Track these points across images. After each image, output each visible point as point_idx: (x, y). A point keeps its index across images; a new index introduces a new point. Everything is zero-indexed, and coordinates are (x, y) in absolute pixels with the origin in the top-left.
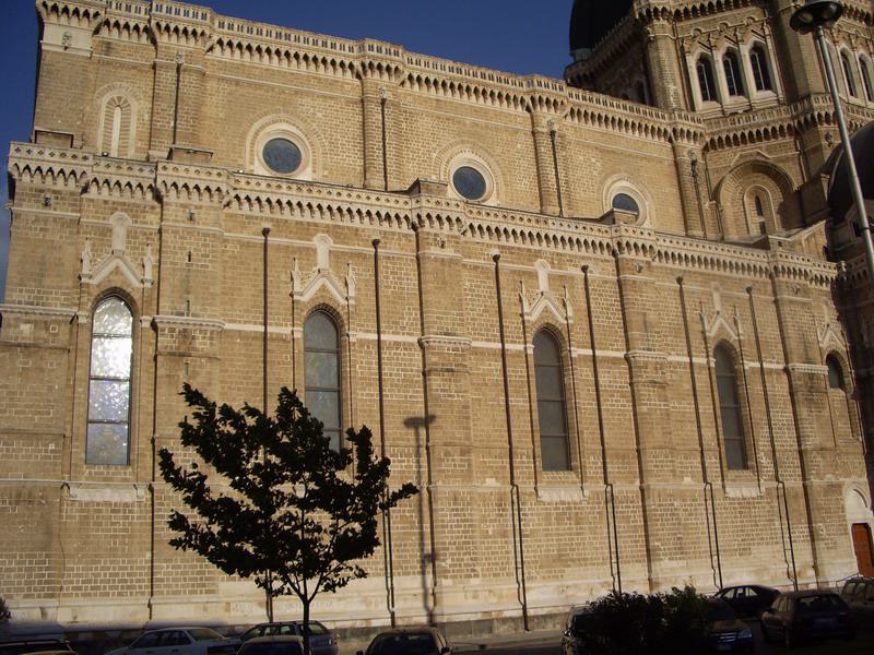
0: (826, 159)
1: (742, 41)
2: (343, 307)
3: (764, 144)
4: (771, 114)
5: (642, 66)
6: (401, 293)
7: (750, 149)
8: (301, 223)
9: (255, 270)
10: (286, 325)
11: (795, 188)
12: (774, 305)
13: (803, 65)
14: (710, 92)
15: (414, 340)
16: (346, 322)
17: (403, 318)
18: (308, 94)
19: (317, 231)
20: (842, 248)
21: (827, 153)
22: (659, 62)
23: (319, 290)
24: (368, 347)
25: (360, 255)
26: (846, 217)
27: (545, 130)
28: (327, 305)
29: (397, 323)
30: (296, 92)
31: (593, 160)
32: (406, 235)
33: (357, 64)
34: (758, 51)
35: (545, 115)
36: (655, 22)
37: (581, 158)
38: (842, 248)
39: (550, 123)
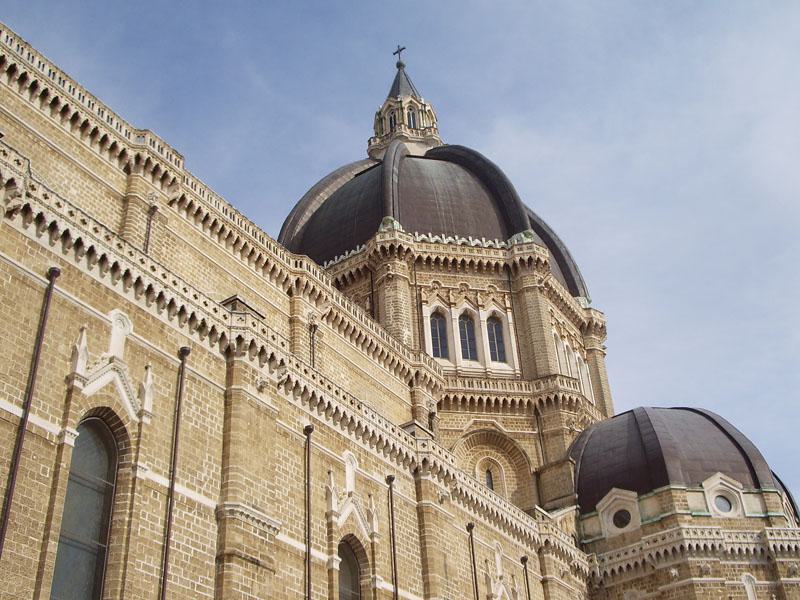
0: (567, 445)
1: (483, 306)
2: (133, 422)
3: (500, 415)
4: (495, 385)
5: (368, 304)
6: (203, 434)
7: (485, 417)
8: (99, 284)
9: (27, 321)
10: (53, 421)
11: (533, 469)
12: (541, 586)
13: (545, 346)
14: (442, 349)
15: (212, 504)
16: (133, 447)
17: (201, 469)
18: (67, 160)
19: (115, 306)
20: (590, 540)
21: (569, 441)
22: (396, 302)
23: (106, 387)
24: (155, 494)
25: (161, 360)
26: (597, 507)
27: (306, 322)
28: (113, 413)
29: (194, 473)
30: (54, 151)
31: (343, 376)
32: (217, 359)
33: (131, 154)
34: (495, 320)
35: (307, 309)
36: (397, 261)
37: (332, 369)
38: (590, 540)
39: (312, 316)
